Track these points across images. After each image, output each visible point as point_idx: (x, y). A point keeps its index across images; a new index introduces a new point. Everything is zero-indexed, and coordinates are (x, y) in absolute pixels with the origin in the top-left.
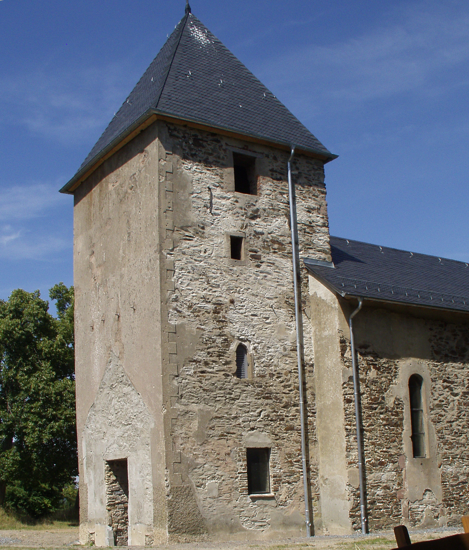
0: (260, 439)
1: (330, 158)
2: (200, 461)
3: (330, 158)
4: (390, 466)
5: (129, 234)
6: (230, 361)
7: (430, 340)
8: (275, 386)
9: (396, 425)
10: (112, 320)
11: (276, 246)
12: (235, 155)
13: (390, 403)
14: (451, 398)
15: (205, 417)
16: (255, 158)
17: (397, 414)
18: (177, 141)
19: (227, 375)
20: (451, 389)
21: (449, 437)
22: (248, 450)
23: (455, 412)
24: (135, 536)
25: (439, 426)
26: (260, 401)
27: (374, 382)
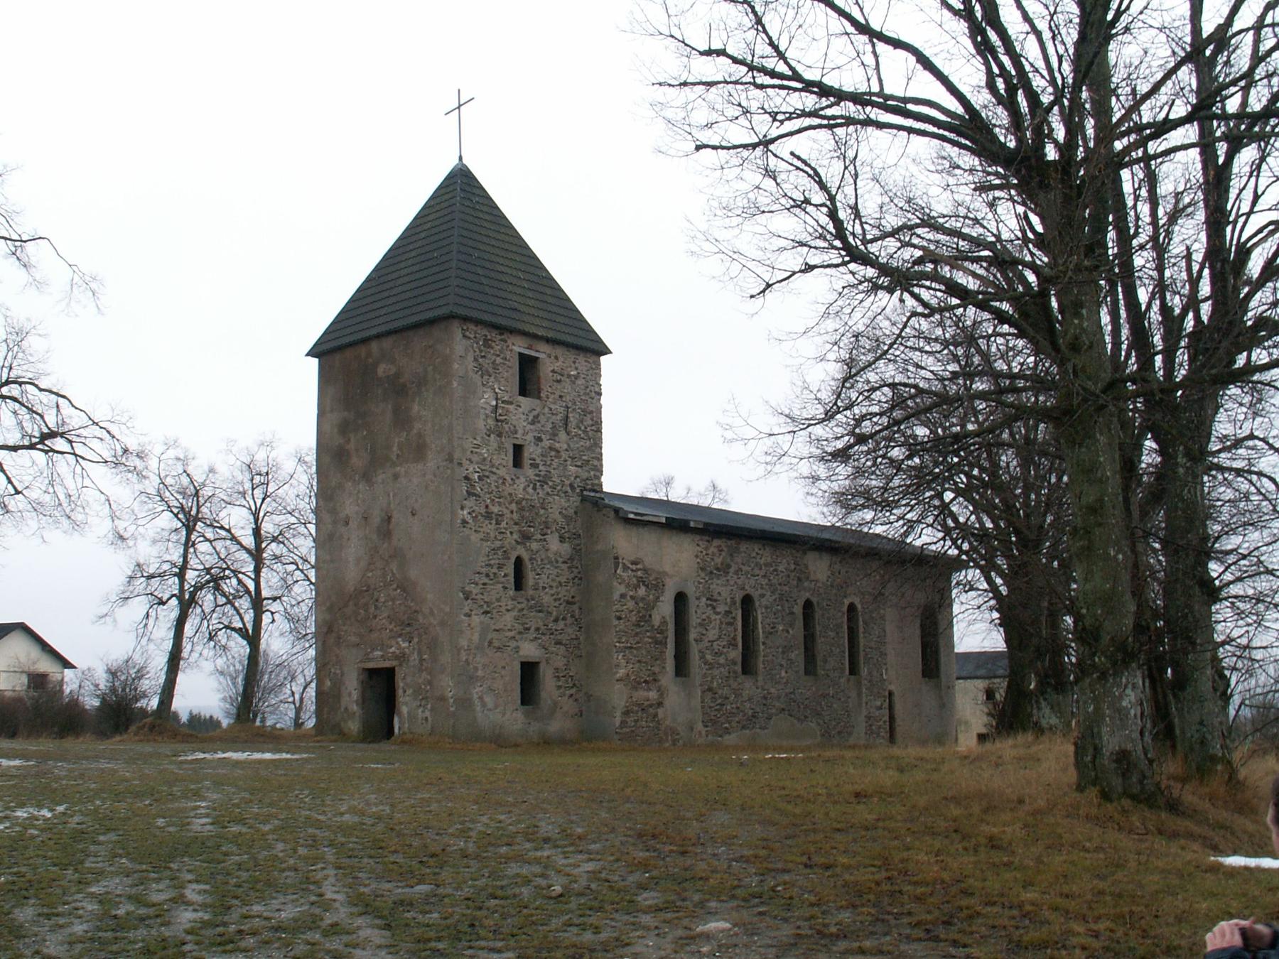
0: (530, 650)
1: (606, 351)
2: (480, 673)
6: (815, 674)
7: (697, 556)
9: (660, 643)
11: (553, 453)
12: (520, 354)
13: (656, 621)
14: (713, 617)
16: (537, 358)
17: (661, 632)
18: (469, 342)
19: (505, 588)
20: (714, 608)
21: (709, 657)
22: (924, 675)
23: (716, 631)
24: (5, 762)
25: (701, 646)
27: (643, 599)
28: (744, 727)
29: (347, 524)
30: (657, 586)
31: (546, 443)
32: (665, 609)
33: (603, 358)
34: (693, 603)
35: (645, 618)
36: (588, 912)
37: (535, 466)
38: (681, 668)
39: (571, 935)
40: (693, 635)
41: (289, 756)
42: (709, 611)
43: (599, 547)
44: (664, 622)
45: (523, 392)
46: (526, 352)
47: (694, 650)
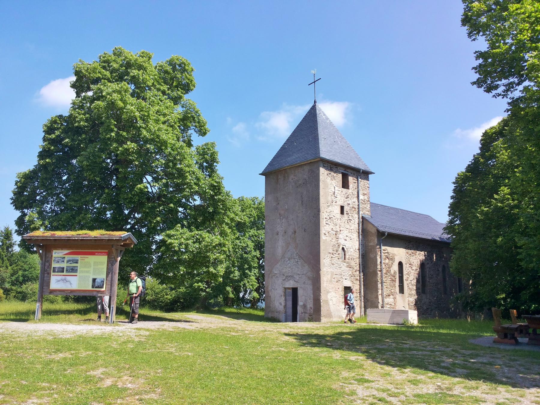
0: (348, 284)
2: (331, 290)
3: (371, 173)
4: (392, 296)
5: (302, 201)
8: (353, 264)
9: (394, 281)
10: (291, 233)
13: (392, 272)
14: (412, 271)
15: (332, 274)
17: (394, 277)
22: (345, 287)
26: (348, 269)
28: (423, 314)
29: (278, 234)
30: (392, 259)
31: (351, 206)
32: (395, 268)
33: (370, 175)
34: (404, 266)
35: (388, 271)
36: (352, 381)
37: (347, 214)
38: (402, 291)
39: (7, 345)
40: (405, 278)
41: (441, 331)
42: (410, 269)
43: (371, 244)
44: (395, 273)
45: (343, 187)
46: (344, 172)
47: (405, 283)
